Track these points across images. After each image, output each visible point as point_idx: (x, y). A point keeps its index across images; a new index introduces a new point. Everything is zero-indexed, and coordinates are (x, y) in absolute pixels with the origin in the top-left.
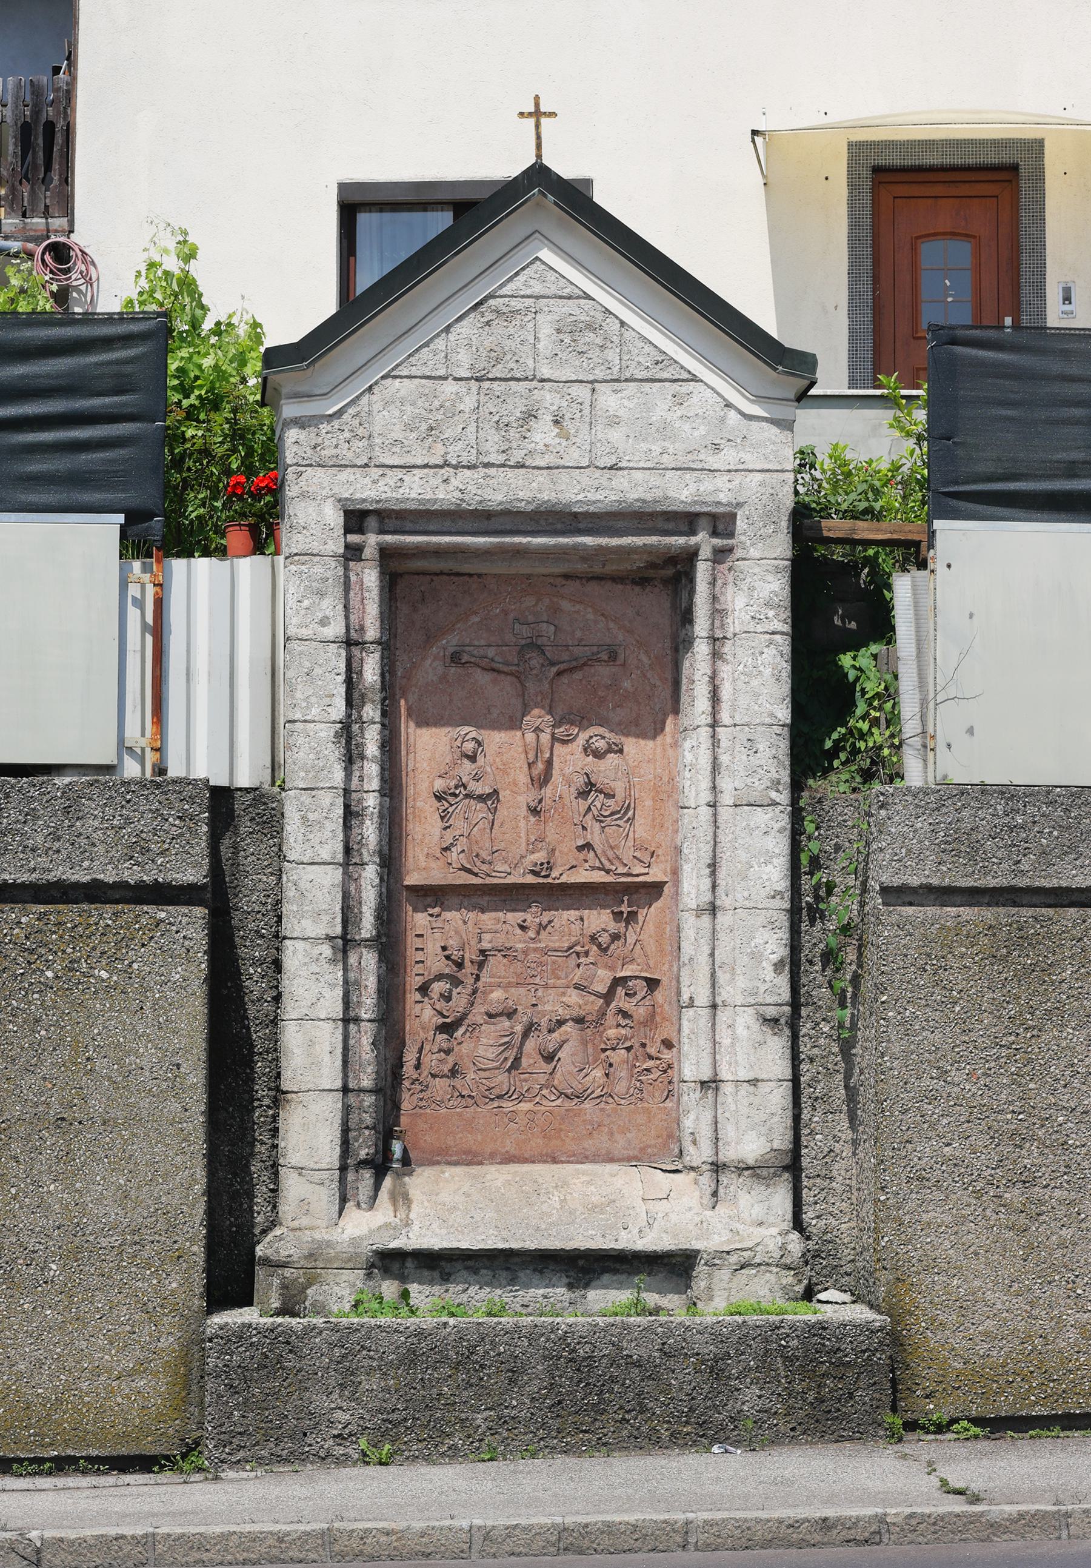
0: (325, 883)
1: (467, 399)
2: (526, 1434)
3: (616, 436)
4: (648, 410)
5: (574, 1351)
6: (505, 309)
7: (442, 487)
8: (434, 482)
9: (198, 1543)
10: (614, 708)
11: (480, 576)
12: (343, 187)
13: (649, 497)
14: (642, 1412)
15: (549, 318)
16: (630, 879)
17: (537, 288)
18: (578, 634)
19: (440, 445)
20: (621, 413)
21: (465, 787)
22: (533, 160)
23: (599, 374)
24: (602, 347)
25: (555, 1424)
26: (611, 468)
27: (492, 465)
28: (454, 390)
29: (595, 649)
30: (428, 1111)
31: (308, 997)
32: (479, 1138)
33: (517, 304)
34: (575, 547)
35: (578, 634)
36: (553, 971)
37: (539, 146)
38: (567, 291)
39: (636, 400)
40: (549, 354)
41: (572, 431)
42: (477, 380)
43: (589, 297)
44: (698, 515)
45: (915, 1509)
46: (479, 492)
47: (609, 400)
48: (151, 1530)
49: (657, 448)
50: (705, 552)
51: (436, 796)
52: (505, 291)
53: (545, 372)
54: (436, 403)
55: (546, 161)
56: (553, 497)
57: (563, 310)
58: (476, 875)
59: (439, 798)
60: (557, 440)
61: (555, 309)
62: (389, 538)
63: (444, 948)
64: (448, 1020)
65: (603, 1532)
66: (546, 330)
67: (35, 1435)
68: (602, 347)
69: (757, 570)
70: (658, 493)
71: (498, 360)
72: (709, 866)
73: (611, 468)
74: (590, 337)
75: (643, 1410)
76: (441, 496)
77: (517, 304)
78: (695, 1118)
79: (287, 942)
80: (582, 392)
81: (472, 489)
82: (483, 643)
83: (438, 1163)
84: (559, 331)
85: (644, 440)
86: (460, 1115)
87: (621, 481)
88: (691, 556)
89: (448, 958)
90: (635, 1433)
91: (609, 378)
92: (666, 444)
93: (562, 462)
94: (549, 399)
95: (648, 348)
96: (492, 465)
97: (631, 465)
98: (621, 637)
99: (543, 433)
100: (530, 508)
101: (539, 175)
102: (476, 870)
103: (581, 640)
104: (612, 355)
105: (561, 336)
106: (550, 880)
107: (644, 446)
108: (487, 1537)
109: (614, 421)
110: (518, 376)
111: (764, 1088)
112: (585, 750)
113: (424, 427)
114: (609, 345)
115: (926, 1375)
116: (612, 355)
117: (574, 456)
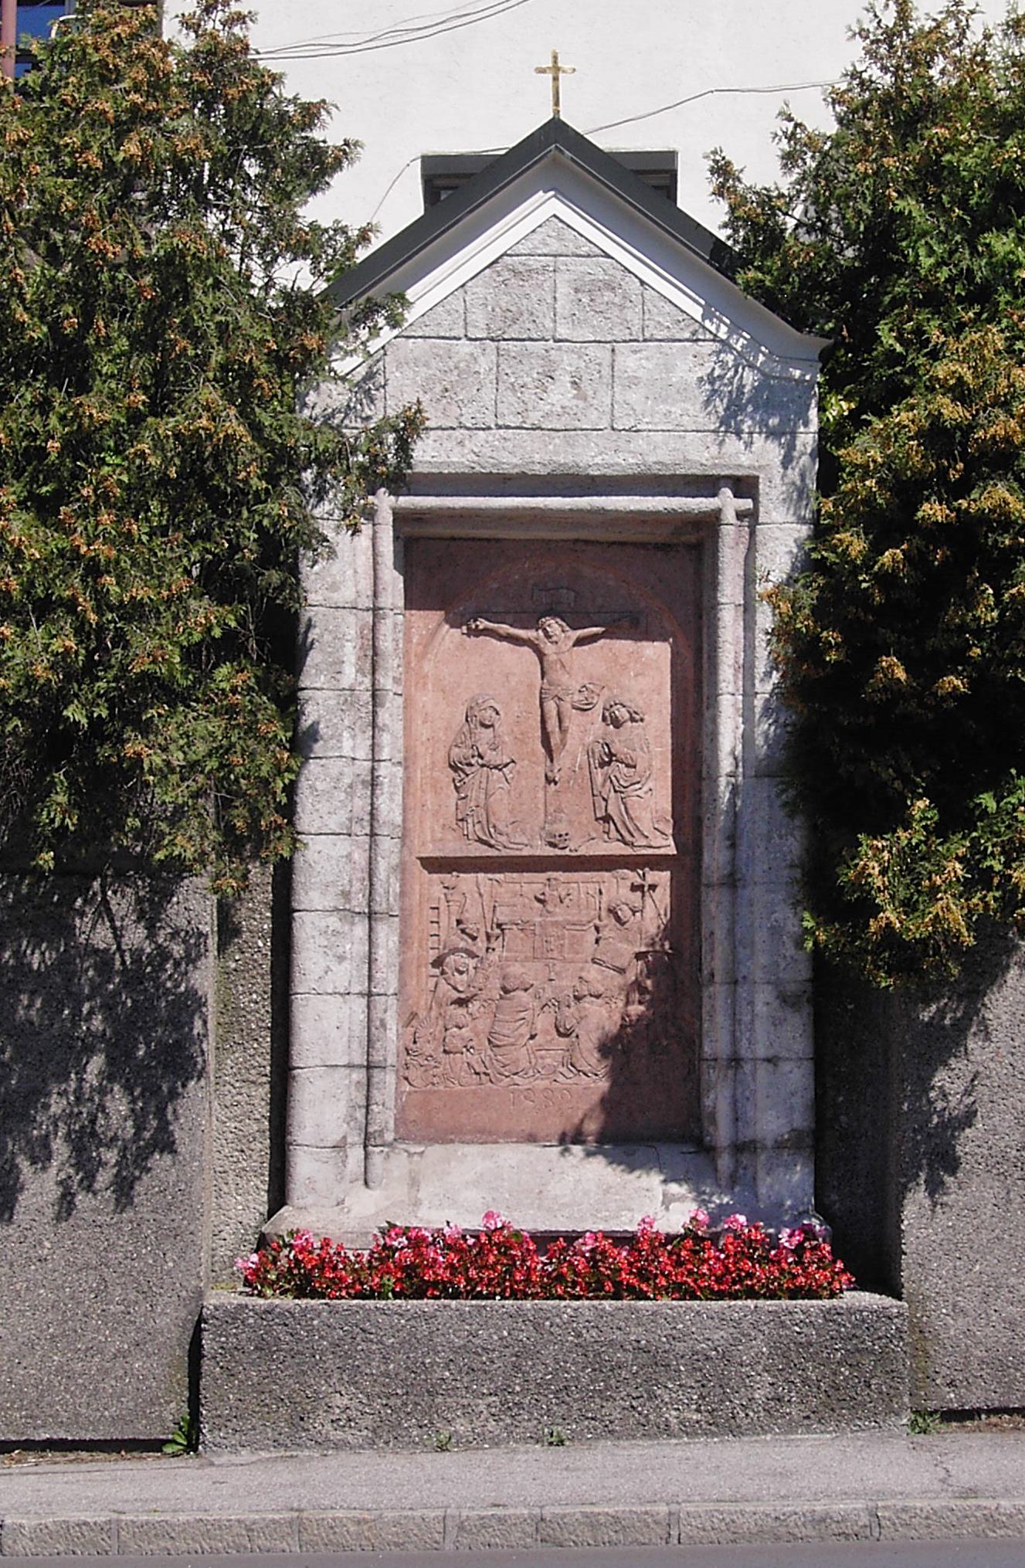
0: (333, 854)
1: (481, 359)
2: (529, 1420)
3: (634, 396)
4: (668, 371)
5: (579, 1335)
6: (521, 268)
7: (458, 449)
8: (448, 445)
9: (164, 1531)
10: (636, 676)
11: (498, 540)
12: (428, 162)
13: (667, 460)
14: (650, 1399)
15: (567, 276)
16: (650, 851)
17: (555, 246)
18: (600, 601)
19: (454, 407)
20: (640, 373)
21: (481, 757)
22: (551, 116)
23: (620, 334)
24: (622, 307)
25: (562, 1410)
26: (629, 430)
27: (508, 427)
28: (467, 350)
29: (616, 616)
30: (441, 1088)
31: (318, 971)
32: (495, 1115)
33: (532, 262)
34: (603, 512)
35: (600, 601)
36: (571, 945)
37: (557, 103)
38: (585, 250)
39: (654, 361)
40: (566, 313)
41: (590, 393)
42: (492, 340)
43: (608, 256)
44: (719, 478)
45: (910, 1503)
46: (494, 455)
47: (629, 361)
48: (115, 1516)
49: (676, 410)
50: (729, 516)
51: (450, 766)
52: (521, 249)
53: (563, 332)
54: (451, 364)
55: (562, 118)
56: (569, 460)
57: (581, 269)
58: (491, 846)
59: (455, 768)
60: (575, 402)
61: (572, 268)
62: (405, 501)
63: (459, 922)
64: (463, 996)
65: (580, 1524)
66: (563, 290)
67: (26, 1417)
68: (622, 307)
69: (778, 534)
70: (678, 457)
71: (515, 321)
72: (728, 838)
73: (629, 430)
74: (608, 296)
75: (653, 1396)
76: (455, 459)
77: (534, 263)
78: (718, 1099)
79: (296, 914)
80: (601, 353)
81: (487, 451)
82: (501, 609)
83: (452, 1141)
84: (577, 291)
85: (664, 401)
86: (474, 1092)
87: (639, 442)
88: (711, 523)
89: (463, 931)
90: (643, 1421)
91: (628, 338)
92: (688, 406)
93: (579, 425)
94: (567, 361)
95: (668, 308)
96: (508, 427)
97: (650, 427)
98: (643, 605)
99: (560, 394)
100: (544, 472)
101: (556, 132)
102: (493, 842)
103: (602, 606)
104: (633, 316)
105: (580, 296)
106: (567, 852)
107: (663, 408)
108: (461, 1528)
109: (634, 382)
110: (535, 336)
111: (786, 1067)
112: (604, 719)
113: (438, 389)
114: (629, 304)
115: (944, 1364)
116: (633, 316)
117: (592, 419)
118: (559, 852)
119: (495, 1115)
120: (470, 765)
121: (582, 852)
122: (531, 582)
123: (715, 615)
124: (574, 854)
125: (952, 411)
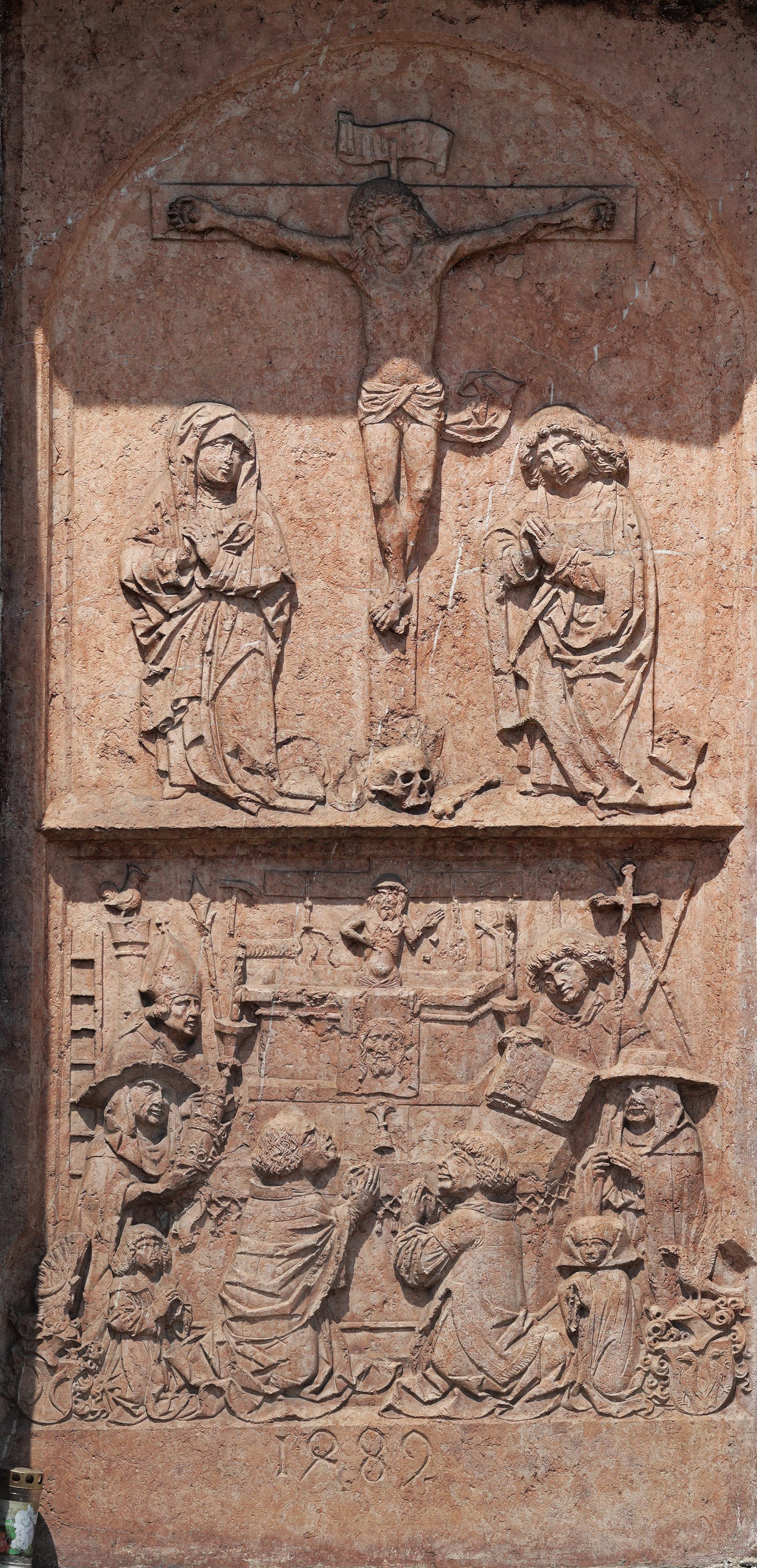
10: (605, 357)
29: (556, 196)
30: (102, 1425)
35: (512, 155)
36: (434, 1061)
58: (233, 803)
63: (148, 998)
64: (157, 1188)
82: (255, 176)
86: (185, 1437)
98: (626, 165)
102: (232, 791)
103: (518, 171)
106: (427, 820)
112: (527, 470)
118: (404, 820)
119: (236, 1496)
120: (178, 590)
121: (464, 818)
122: (333, 102)
123: (274, 413)
124: (447, 823)
125: (588, 445)
